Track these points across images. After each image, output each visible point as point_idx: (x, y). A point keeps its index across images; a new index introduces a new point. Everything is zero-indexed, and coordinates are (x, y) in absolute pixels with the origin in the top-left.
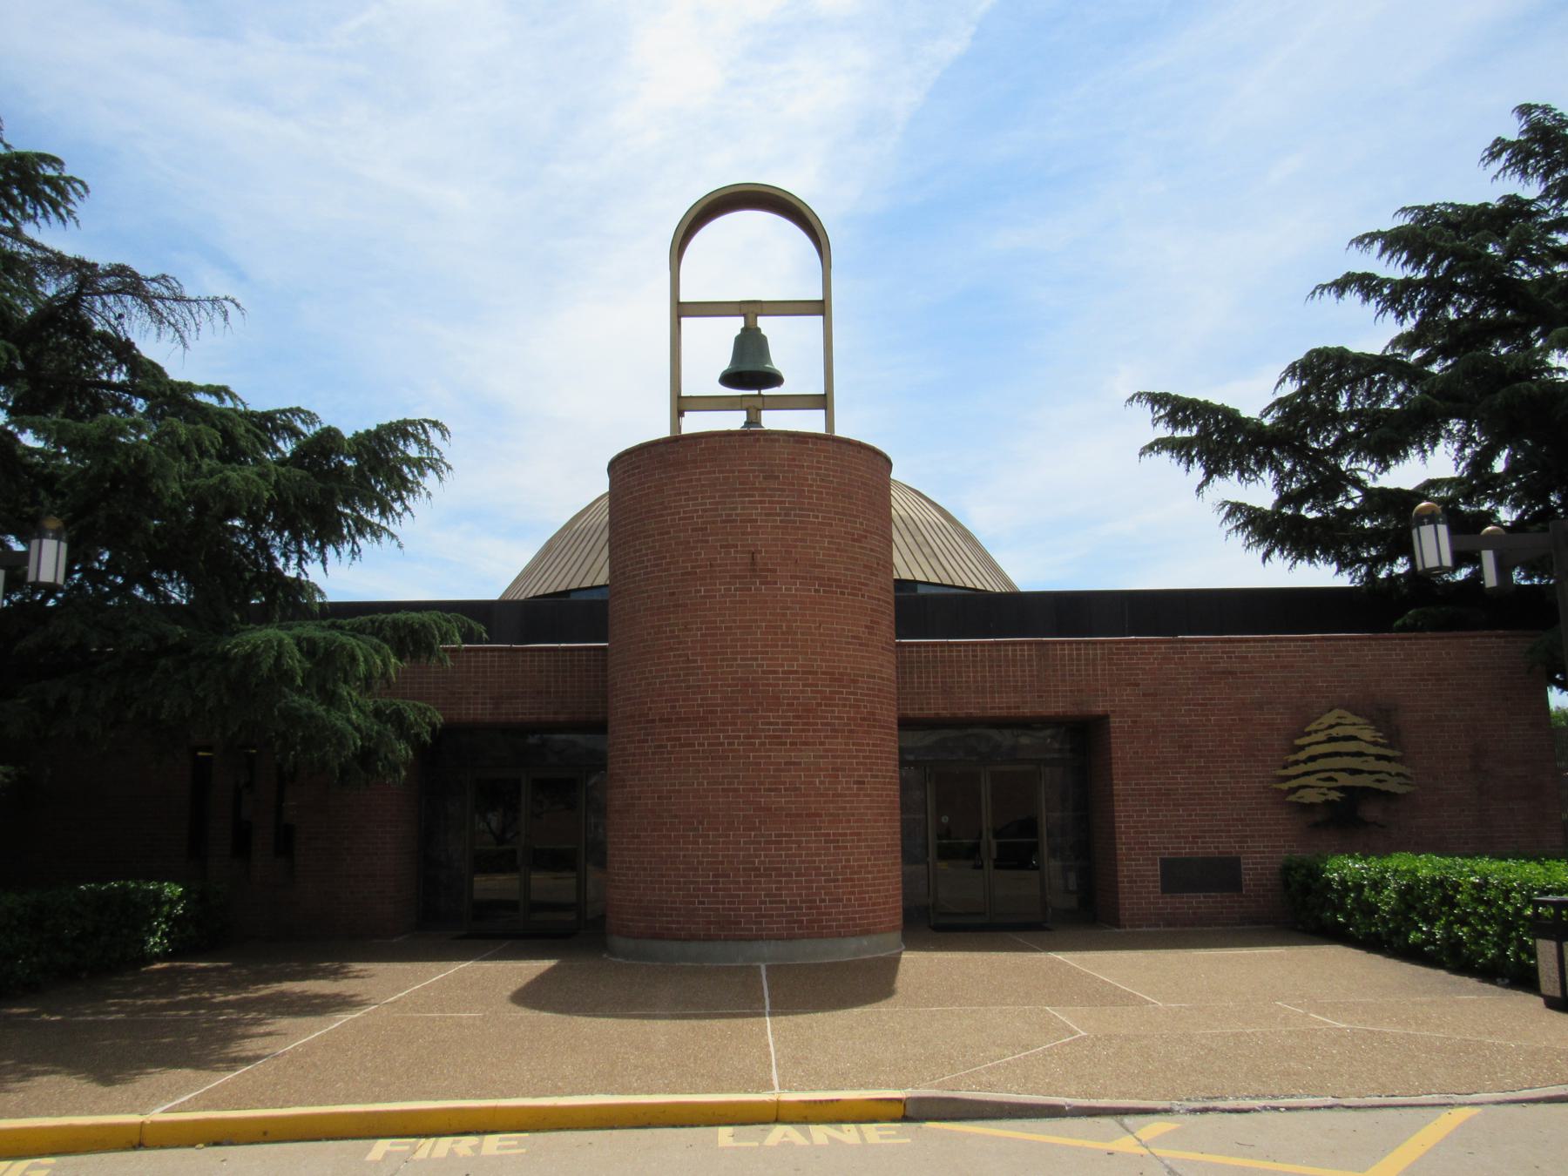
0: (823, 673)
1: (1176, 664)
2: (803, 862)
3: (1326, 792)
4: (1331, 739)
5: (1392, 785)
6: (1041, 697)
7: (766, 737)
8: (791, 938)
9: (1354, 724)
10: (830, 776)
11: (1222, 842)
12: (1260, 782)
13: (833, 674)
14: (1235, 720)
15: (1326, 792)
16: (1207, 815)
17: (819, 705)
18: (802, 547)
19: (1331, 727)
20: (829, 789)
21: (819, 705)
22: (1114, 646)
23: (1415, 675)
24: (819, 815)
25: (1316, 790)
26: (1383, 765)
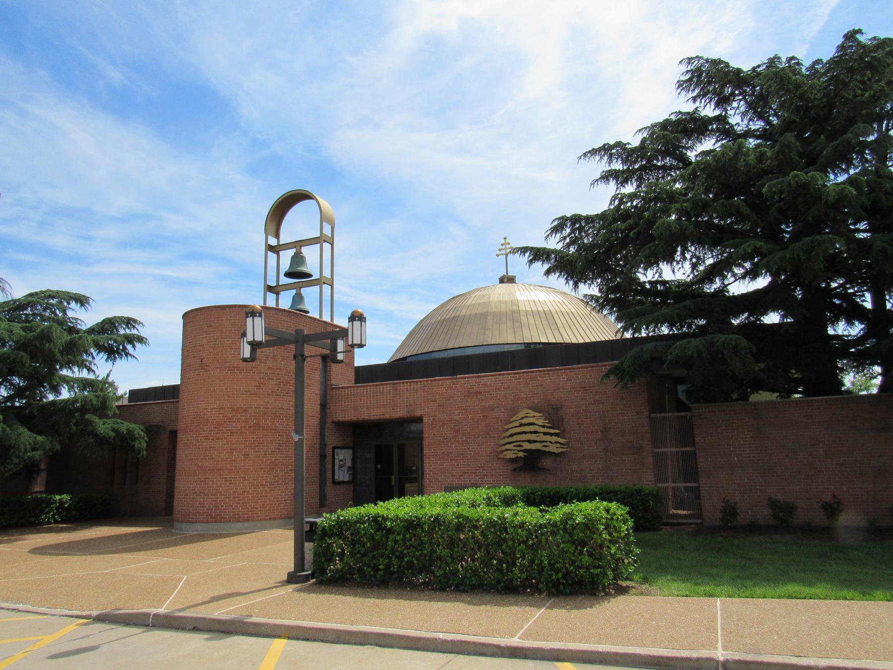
0: (229, 408)
1: (453, 390)
2: (214, 490)
3: (517, 452)
4: (521, 425)
5: (553, 448)
6: (393, 409)
7: (203, 437)
8: (207, 522)
9: (534, 417)
10: (228, 452)
11: (473, 478)
12: (492, 448)
13: (233, 408)
14: (480, 416)
15: (517, 452)
16: (466, 465)
17: (225, 422)
18: (221, 355)
19: (522, 418)
20: (228, 458)
21: (225, 422)
22: (426, 383)
23: (572, 388)
24: (222, 470)
25: (513, 452)
26: (548, 438)
